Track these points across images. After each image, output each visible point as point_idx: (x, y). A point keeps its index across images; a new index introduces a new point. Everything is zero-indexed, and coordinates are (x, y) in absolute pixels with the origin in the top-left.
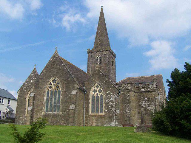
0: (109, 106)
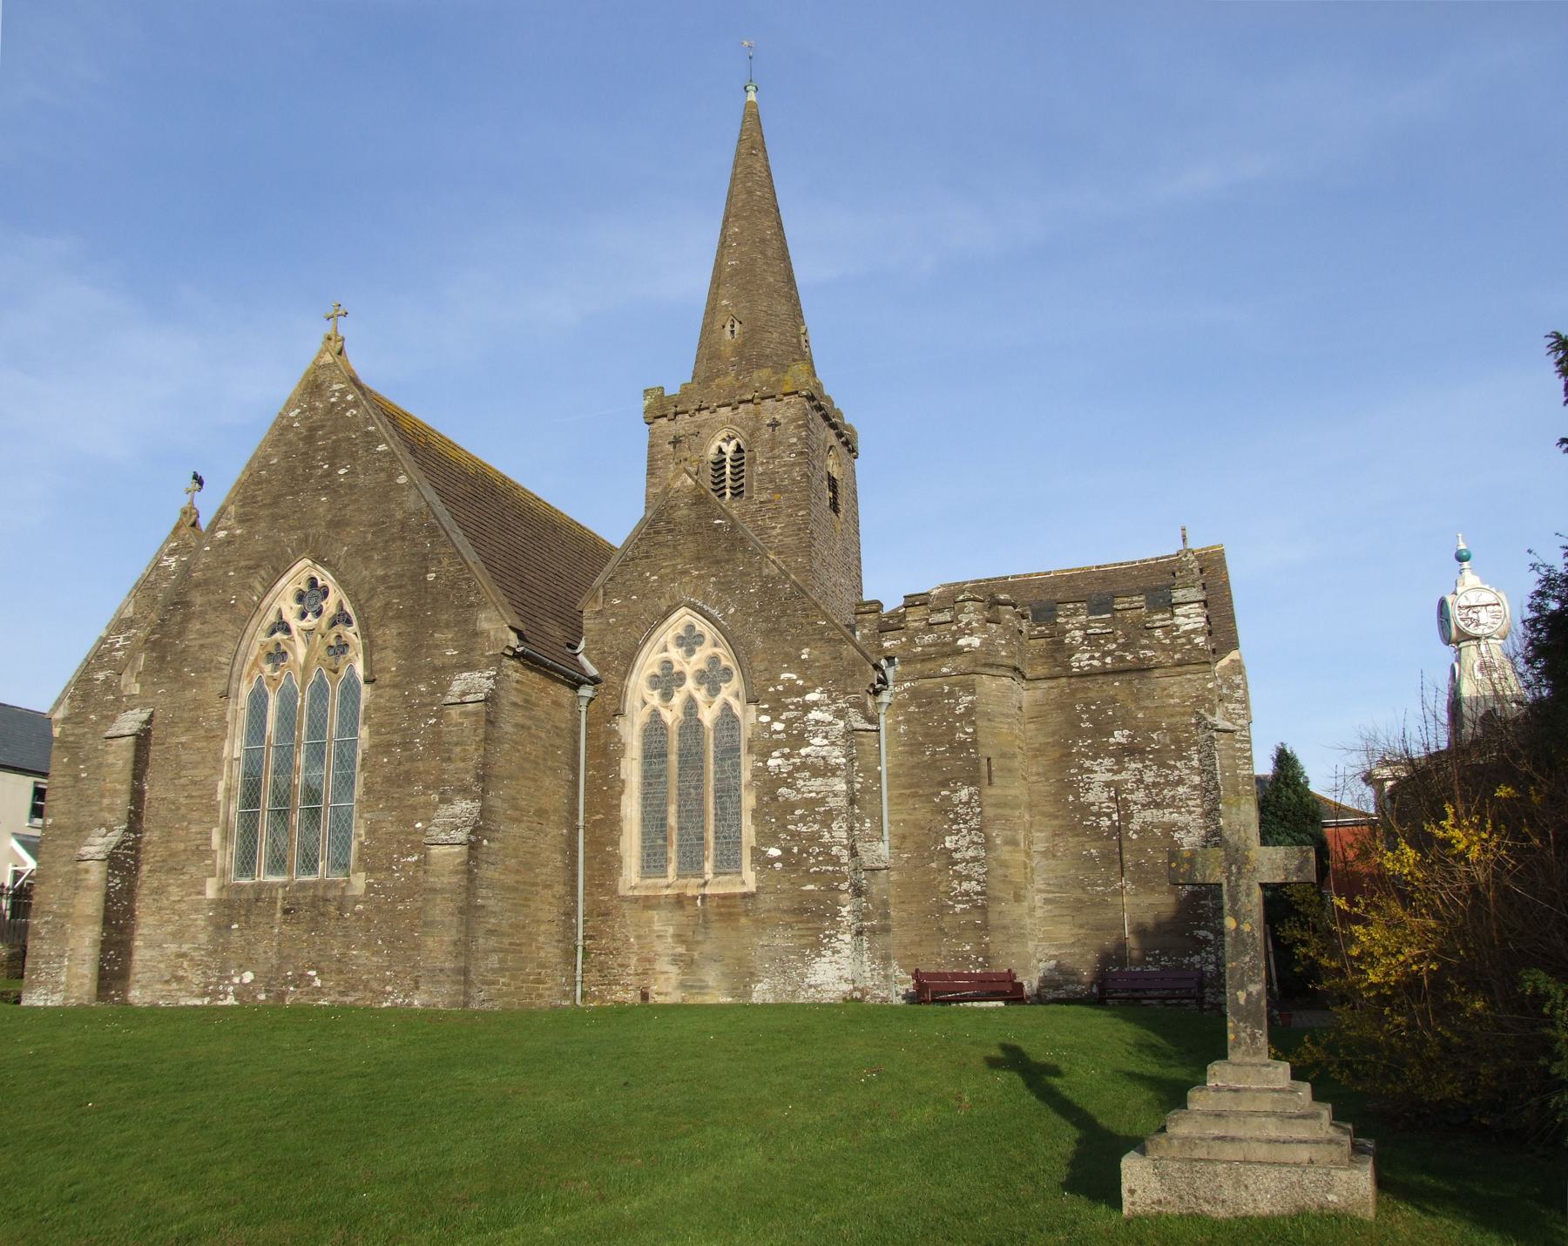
0: (790, 807)
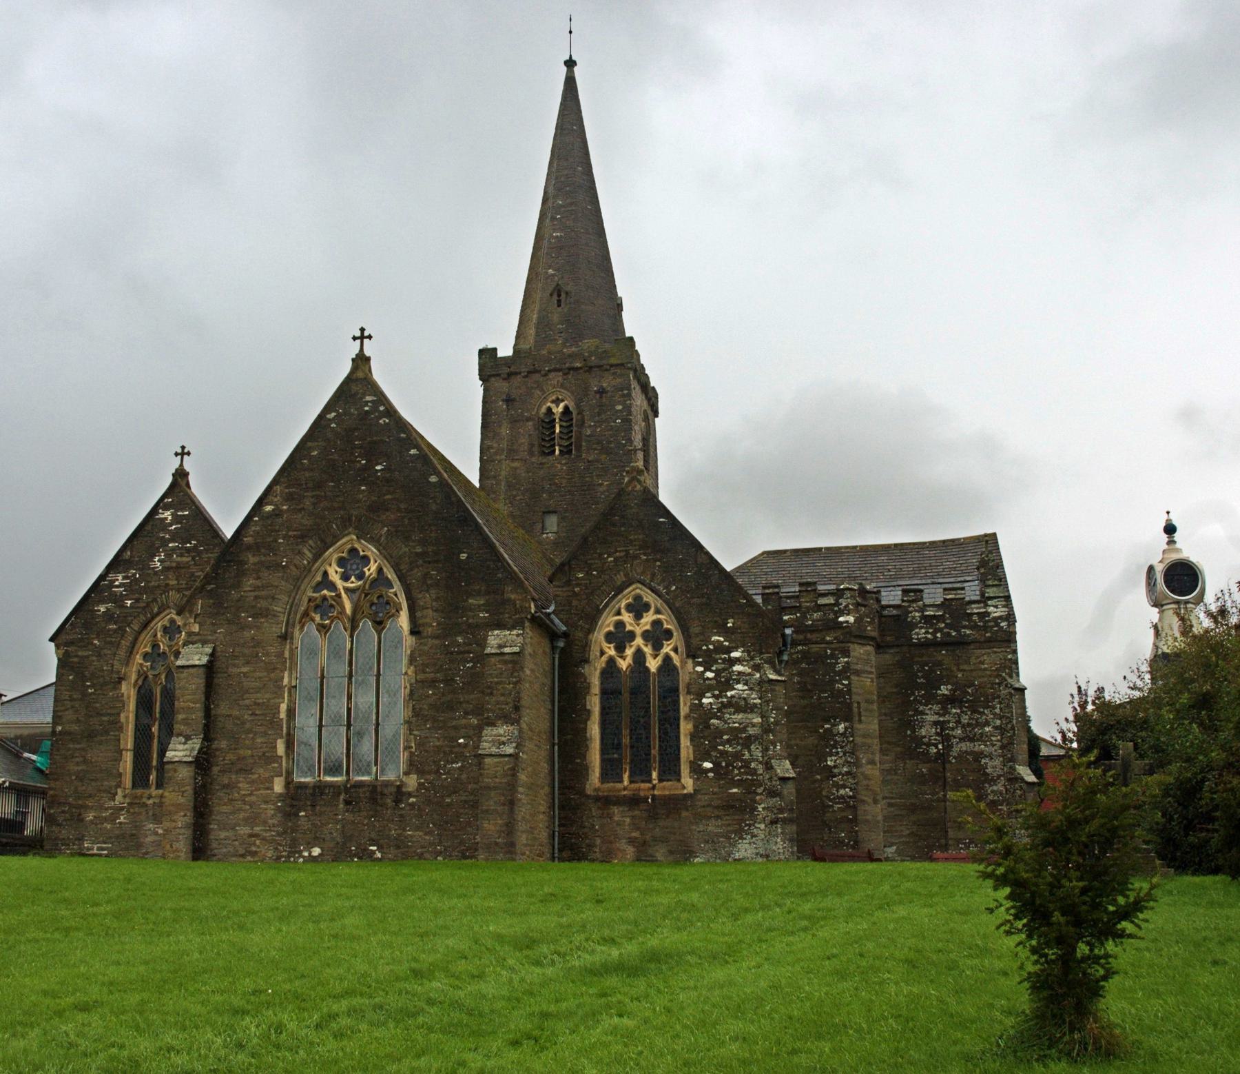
0: (719, 733)
